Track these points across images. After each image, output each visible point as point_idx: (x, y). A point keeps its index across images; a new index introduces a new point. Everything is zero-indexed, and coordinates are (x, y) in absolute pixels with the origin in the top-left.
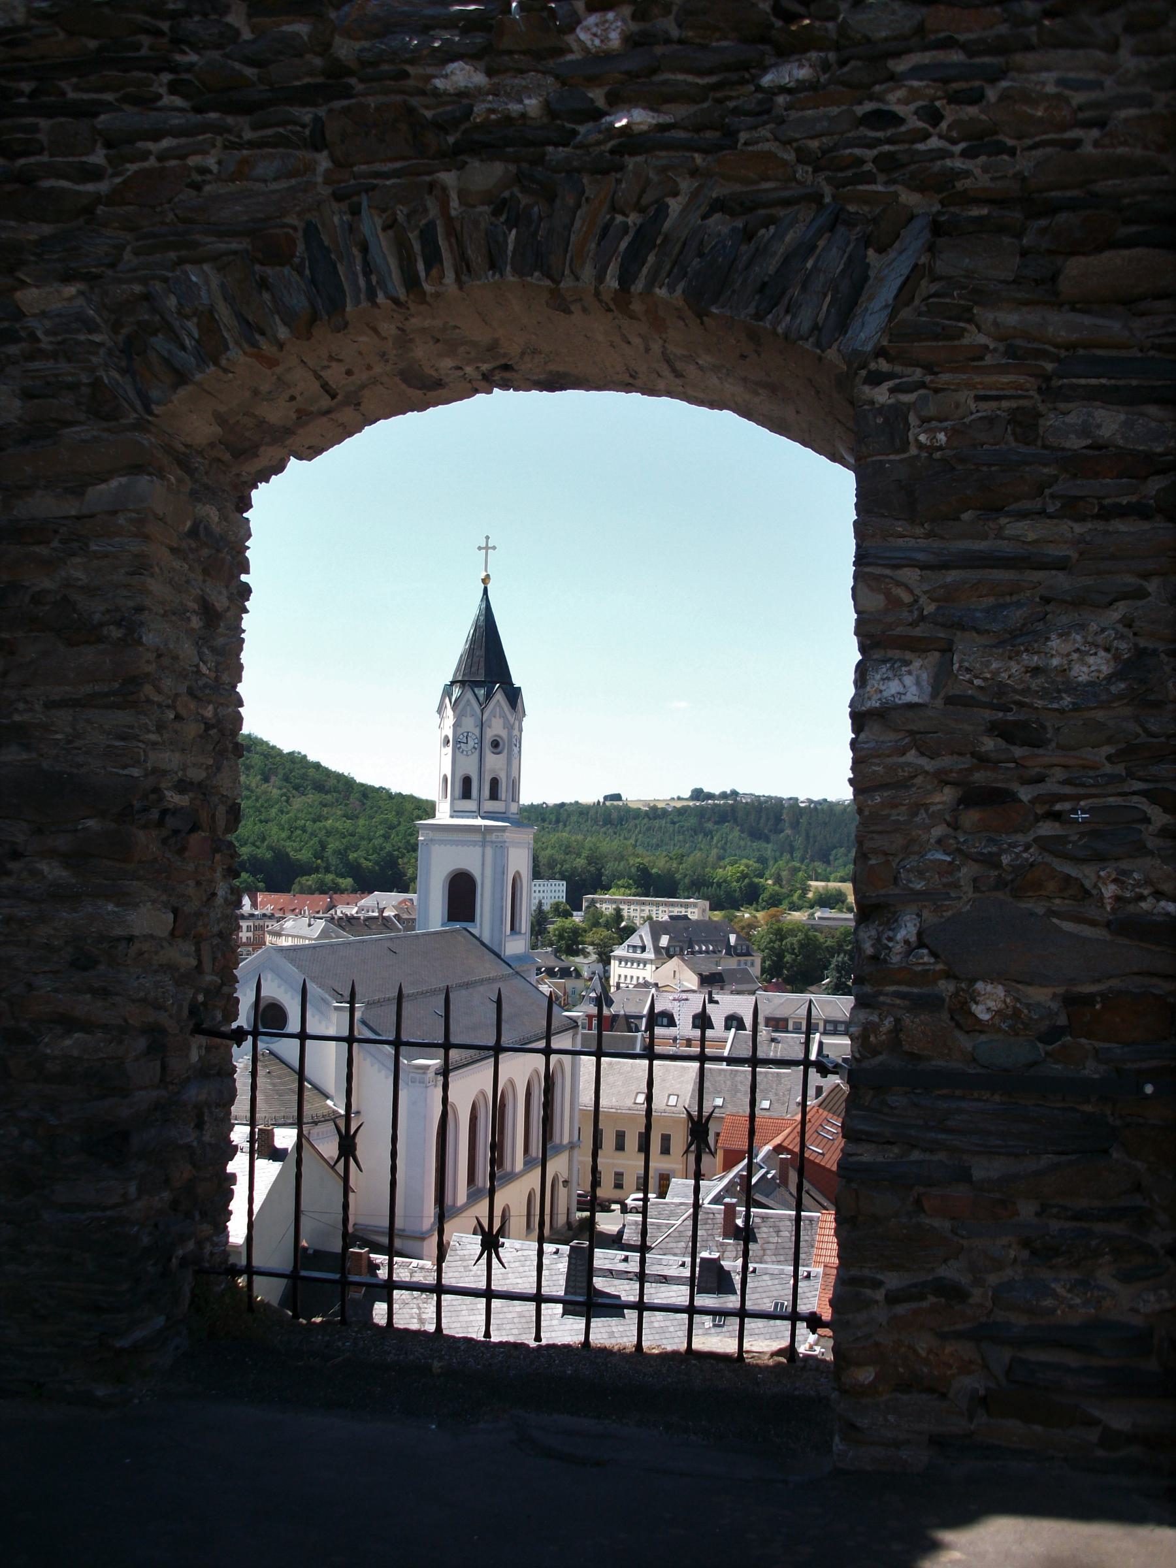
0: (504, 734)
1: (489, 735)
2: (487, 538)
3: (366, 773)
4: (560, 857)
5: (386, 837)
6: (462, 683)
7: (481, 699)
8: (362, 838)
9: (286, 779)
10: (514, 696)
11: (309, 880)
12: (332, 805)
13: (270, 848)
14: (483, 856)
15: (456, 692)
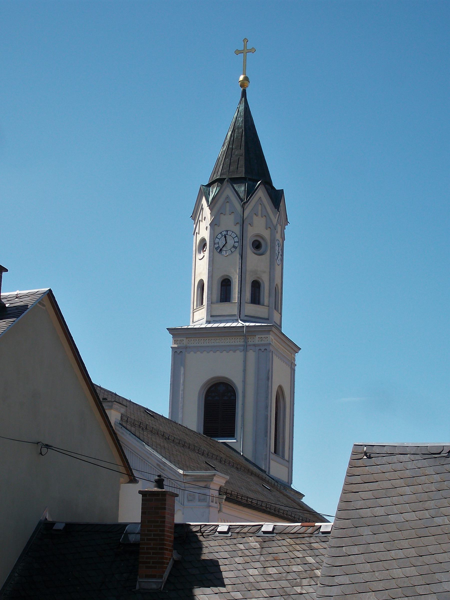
0: (266, 234)
7: (242, 195)
10: (277, 197)
14: (245, 361)
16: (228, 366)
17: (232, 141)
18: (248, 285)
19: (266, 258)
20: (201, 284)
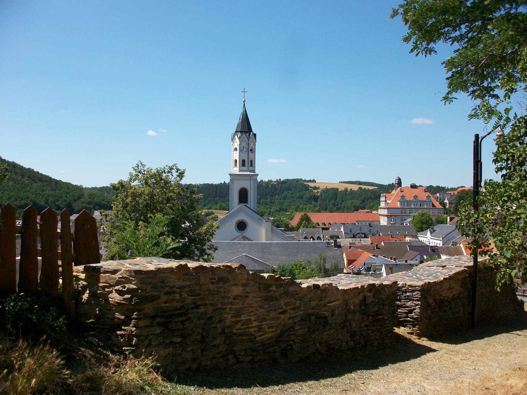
0: (253, 147)
1: (250, 147)
6: (241, 132)
9: (29, 177)
10: (255, 135)
12: (47, 186)
13: (31, 201)
15: (239, 135)
17: (242, 120)
20: (236, 161)
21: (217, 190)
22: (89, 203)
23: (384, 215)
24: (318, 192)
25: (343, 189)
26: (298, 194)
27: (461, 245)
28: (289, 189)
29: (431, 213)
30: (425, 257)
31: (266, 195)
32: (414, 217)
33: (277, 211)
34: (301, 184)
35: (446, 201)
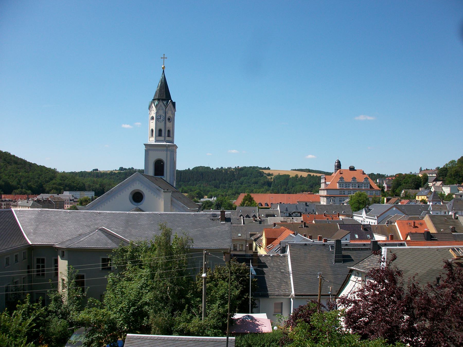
0: (171, 116)
2: (164, 55)
3: (30, 159)
4: (91, 184)
5: (39, 178)
6: (159, 100)
8: (31, 179)
9: (5, 160)
10: (174, 104)
11: (17, 191)
13: (3, 181)
14: (167, 154)
15: (156, 102)
16: (162, 156)
17: (161, 87)
18: (165, 131)
19: (171, 123)
20: (152, 130)
21: (181, 175)
22: (60, 184)
23: (323, 196)
24: (271, 178)
25: (294, 176)
26: (254, 180)
27: (396, 224)
28: (245, 175)
29: (369, 194)
30: (357, 236)
31: (225, 180)
32: (351, 197)
33: (233, 194)
34: (257, 171)
35: (385, 185)
